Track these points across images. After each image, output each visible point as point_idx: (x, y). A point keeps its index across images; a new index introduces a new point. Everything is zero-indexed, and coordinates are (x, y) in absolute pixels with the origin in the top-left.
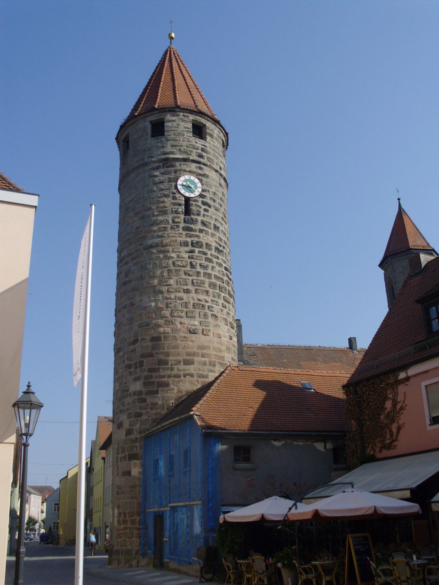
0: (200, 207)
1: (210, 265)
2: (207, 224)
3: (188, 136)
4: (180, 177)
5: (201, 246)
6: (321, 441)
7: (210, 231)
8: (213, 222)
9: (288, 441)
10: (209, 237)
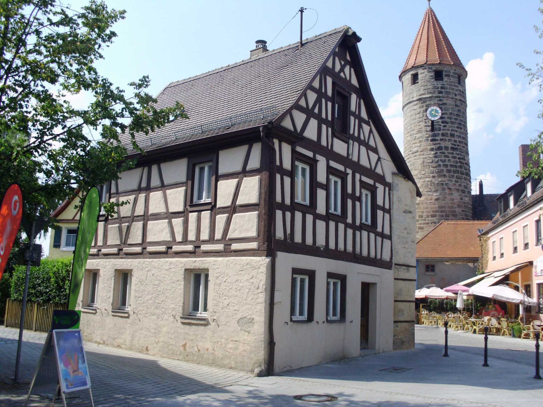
0: (441, 125)
1: (447, 159)
2: (446, 134)
5: (441, 149)
6: (472, 262)
7: (447, 138)
8: (449, 132)
9: (453, 262)
10: (447, 142)
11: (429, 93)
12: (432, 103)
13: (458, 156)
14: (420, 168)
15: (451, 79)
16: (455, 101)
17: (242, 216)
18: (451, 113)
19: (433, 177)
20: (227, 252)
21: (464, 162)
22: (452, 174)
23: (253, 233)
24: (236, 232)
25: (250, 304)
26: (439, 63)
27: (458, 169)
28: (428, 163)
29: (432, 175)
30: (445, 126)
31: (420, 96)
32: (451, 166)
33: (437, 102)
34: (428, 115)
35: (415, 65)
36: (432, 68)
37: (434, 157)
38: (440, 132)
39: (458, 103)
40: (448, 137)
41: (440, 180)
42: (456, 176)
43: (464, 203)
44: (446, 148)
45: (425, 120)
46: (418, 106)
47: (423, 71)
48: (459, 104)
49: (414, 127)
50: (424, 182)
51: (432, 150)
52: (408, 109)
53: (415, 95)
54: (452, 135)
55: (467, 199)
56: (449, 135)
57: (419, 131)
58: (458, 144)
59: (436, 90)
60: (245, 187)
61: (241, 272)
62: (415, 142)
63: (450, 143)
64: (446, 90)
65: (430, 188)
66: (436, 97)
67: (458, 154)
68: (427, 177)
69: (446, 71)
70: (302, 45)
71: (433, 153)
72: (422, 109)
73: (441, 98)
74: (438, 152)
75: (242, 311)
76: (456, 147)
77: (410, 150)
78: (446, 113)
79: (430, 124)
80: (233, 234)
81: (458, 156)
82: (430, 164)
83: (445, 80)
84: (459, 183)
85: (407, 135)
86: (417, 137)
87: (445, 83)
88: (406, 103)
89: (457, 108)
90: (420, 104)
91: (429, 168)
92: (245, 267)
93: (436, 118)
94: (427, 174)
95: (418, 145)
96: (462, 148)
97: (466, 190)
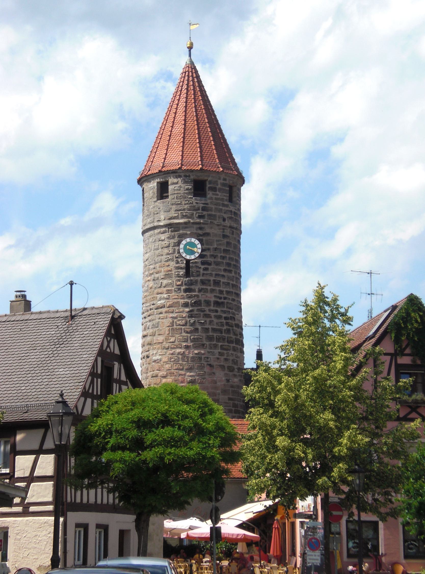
0: (200, 268)
1: (208, 320)
2: (206, 282)
3: (189, 198)
4: (182, 241)
7: (209, 288)
8: (212, 279)
10: (209, 295)
11: (183, 217)
12: (189, 232)
13: (224, 315)
14: (167, 333)
15: (217, 195)
16: (223, 229)
17: (39, 485)
18: (216, 249)
19: (187, 347)
20: (26, 513)
21: (234, 323)
22: (215, 342)
23: (50, 498)
24: (34, 498)
25: (48, 553)
26: (201, 169)
27: (223, 334)
28: (179, 325)
29: (184, 344)
30: (206, 269)
31: (169, 219)
32: (214, 330)
33: (195, 231)
34: (181, 251)
35: (164, 169)
36: (189, 176)
37: (189, 317)
38: (199, 279)
39: (228, 232)
40: (210, 286)
41: (196, 352)
42: (221, 346)
43: (232, 386)
44: (208, 303)
45: (177, 258)
46: (167, 235)
47: (175, 180)
48: (228, 234)
49: (159, 267)
50: (172, 354)
51: (186, 305)
52: (150, 236)
53: (162, 217)
54: (217, 283)
55: (236, 380)
56: (212, 282)
57: (168, 276)
58: (225, 296)
60: (43, 462)
61: (39, 529)
62: (160, 290)
63: (213, 295)
64: (210, 213)
65: (181, 365)
66: (193, 223)
67: (224, 312)
68: (177, 348)
69: (210, 182)
70: (72, 317)
71: (187, 310)
72: (172, 241)
73: (203, 226)
74: (195, 308)
75: (41, 559)
76: (222, 300)
77: (152, 303)
78: (209, 249)
79: (183, 265)
80: (32, 499)
81: (224, 315)
82: (183, 327)
83: (208, 196)
84: (225, 357)
85: (149, 278)
86: (164, 285)
87: (209, 201)
88: (148, 226)
89: (225, 240)
91: (181, 333)
92: (42, 525)
93: (193, 257)
94: (177, 343)
95: (165, 296)
96: (230, 301)
97: (236, 367)
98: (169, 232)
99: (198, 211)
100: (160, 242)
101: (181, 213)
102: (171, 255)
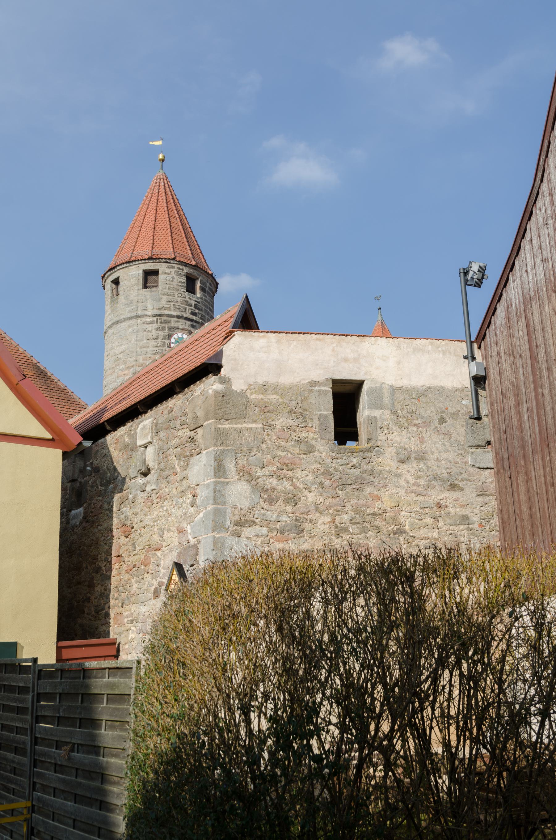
4: (173, 335)
11: (176, 309)
15: (206, 297)
46: (155, 326)
49: (143, 360)
53: (150, 307)
59: (188, 307)
72: (161, 333)
90: (159, 324)
98: (157, 323)
99: (191, 308)
100: (145, 333)
101: (174, 305)
102: (160, 348)
